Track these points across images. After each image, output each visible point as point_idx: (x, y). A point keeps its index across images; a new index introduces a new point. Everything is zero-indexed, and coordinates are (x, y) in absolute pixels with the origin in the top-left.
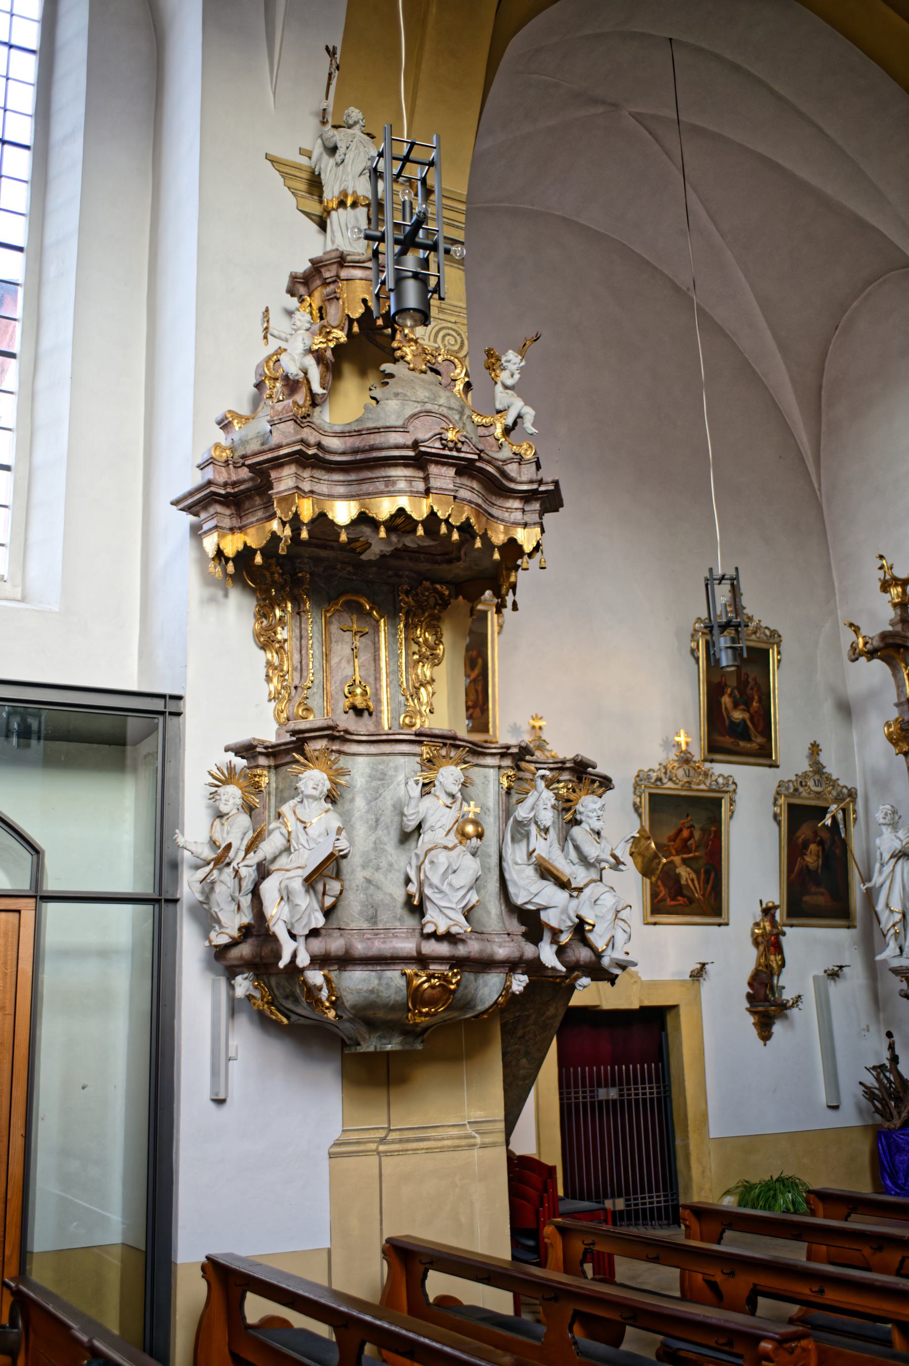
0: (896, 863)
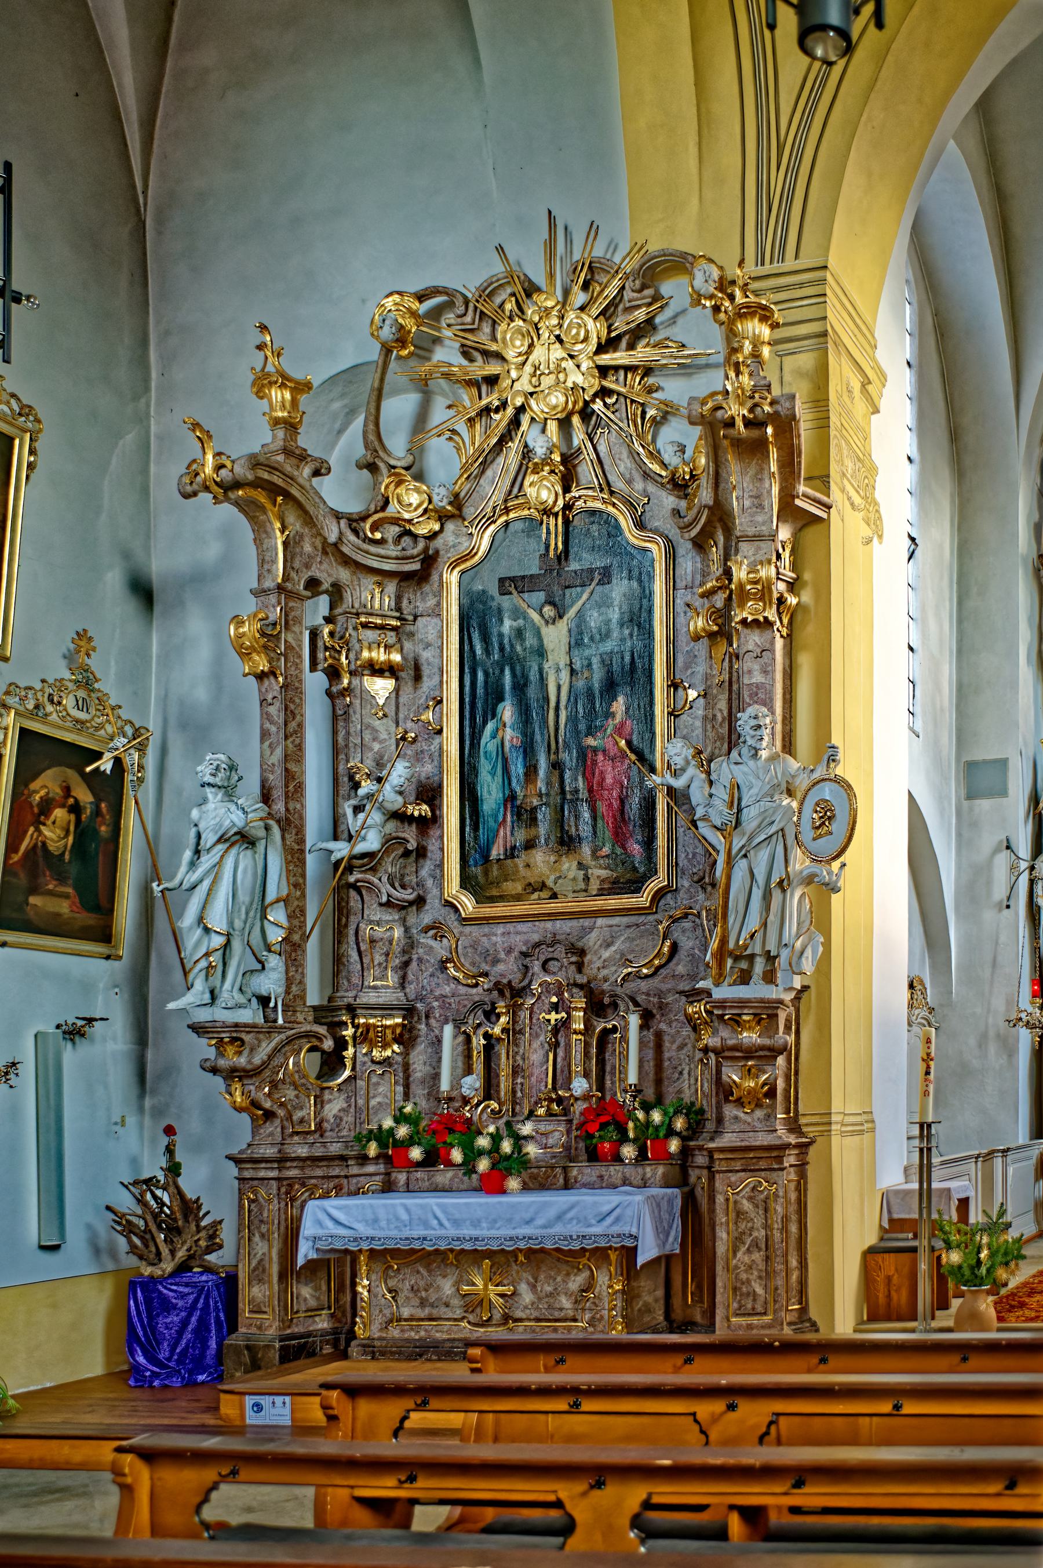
0: (226, 851)
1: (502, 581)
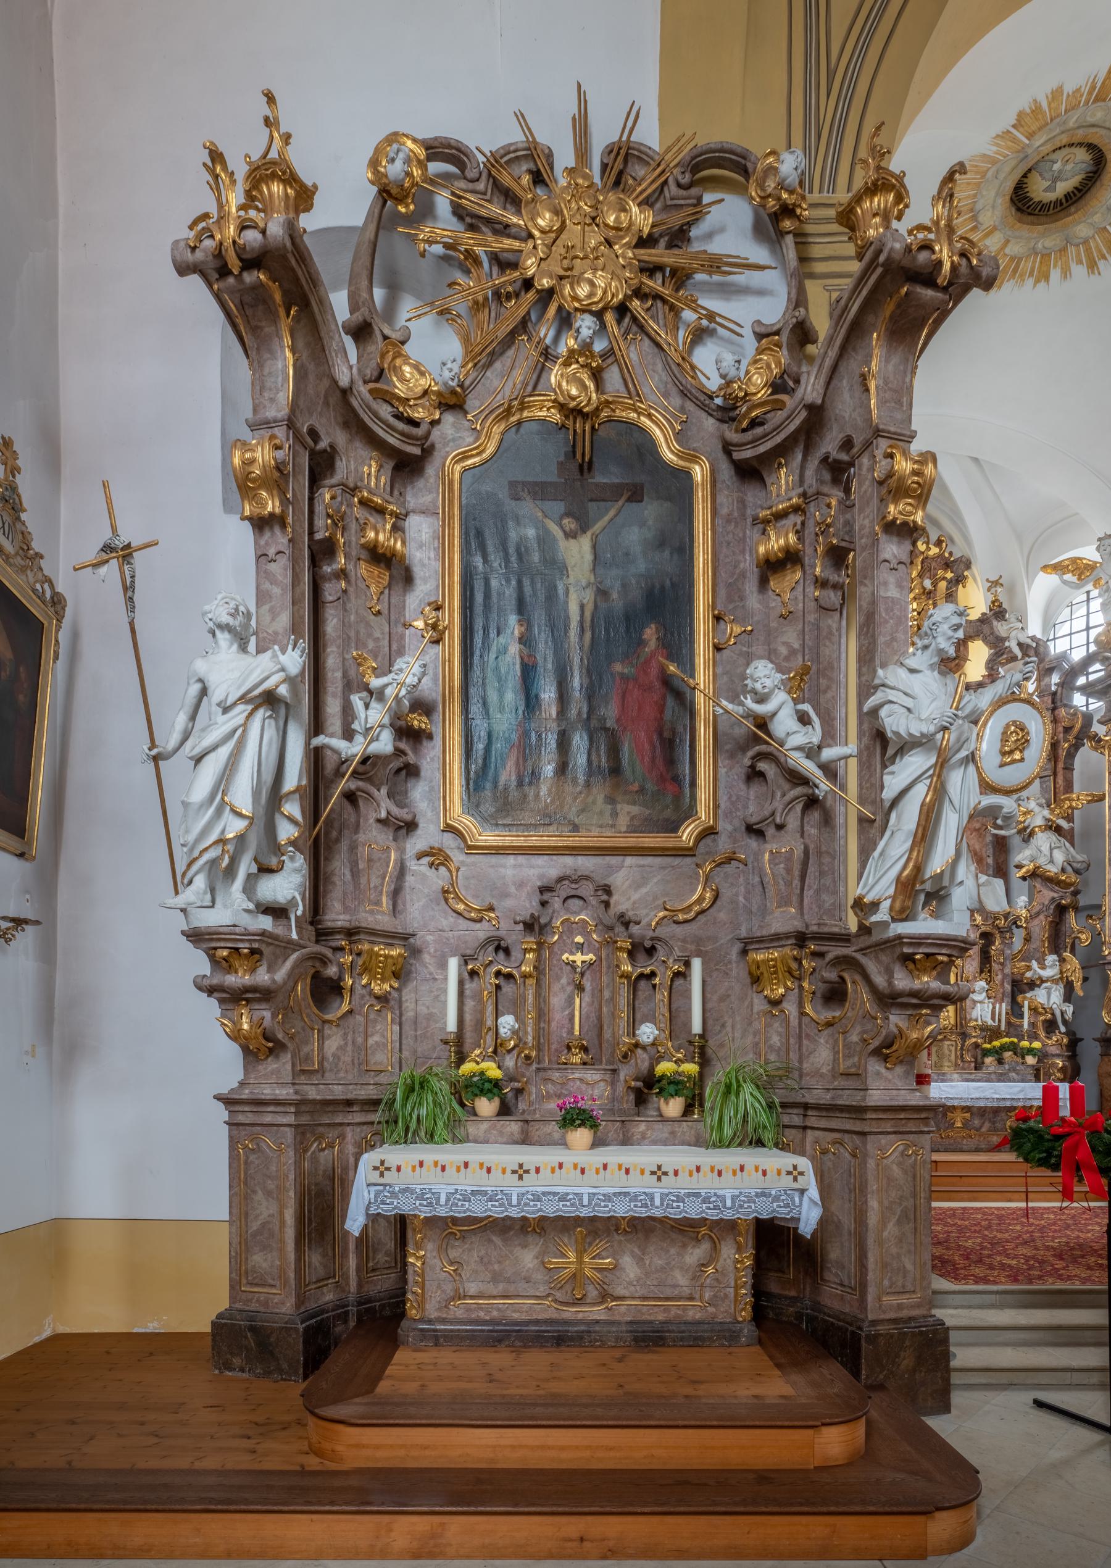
0: (251, 714)
1: (513, 484)
